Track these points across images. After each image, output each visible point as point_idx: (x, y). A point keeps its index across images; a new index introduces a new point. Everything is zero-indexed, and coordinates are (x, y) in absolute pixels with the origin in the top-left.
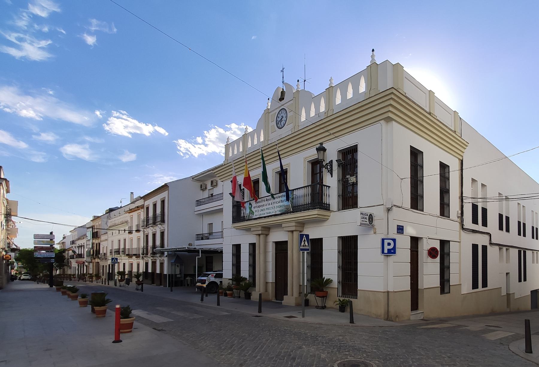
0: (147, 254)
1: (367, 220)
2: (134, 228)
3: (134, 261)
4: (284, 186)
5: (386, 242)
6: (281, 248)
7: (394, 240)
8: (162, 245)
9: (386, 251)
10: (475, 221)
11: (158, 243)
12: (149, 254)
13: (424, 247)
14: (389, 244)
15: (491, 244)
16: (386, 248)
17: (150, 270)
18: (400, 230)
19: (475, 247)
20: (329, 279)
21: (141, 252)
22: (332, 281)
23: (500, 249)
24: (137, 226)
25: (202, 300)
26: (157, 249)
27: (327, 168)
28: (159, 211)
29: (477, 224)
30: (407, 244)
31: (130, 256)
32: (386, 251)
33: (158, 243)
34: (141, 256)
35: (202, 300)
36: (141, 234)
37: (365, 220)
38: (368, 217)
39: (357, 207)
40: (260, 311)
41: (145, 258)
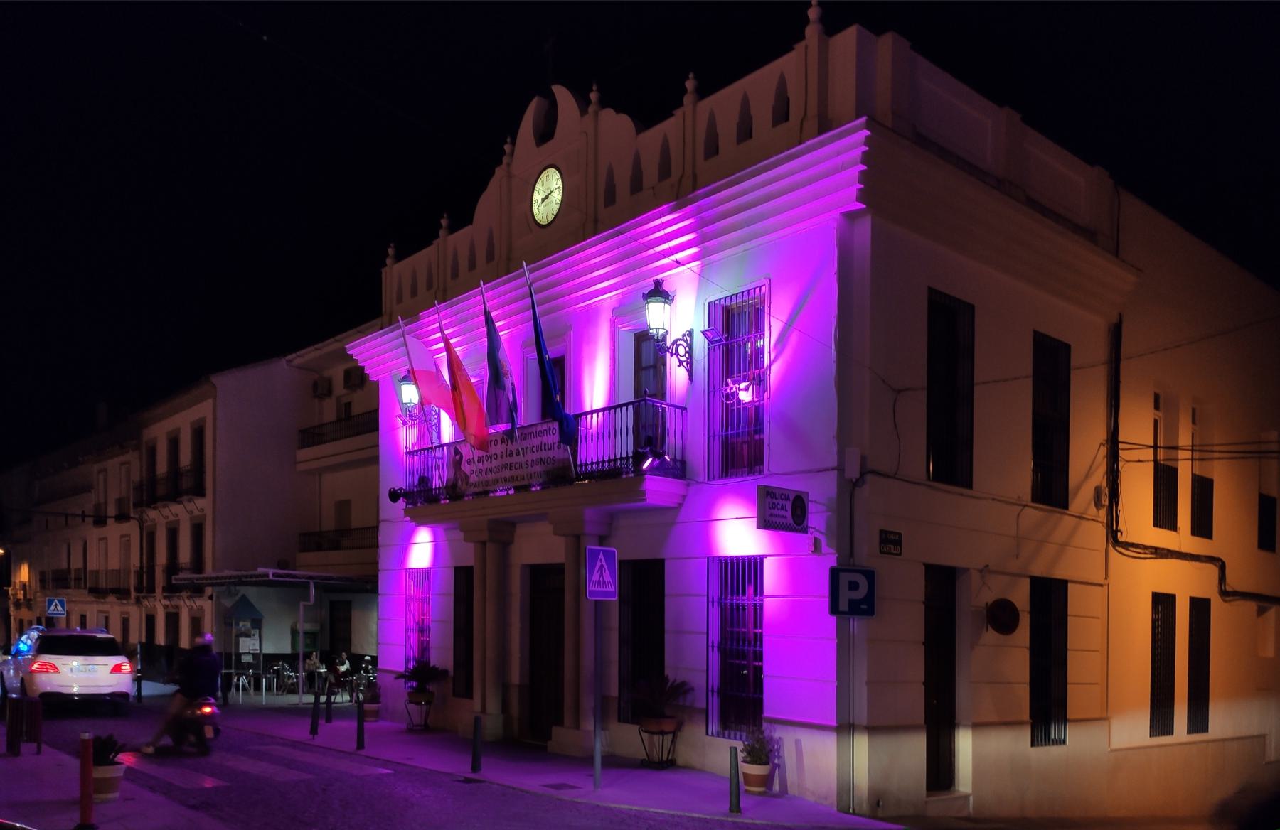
0: (151, 590)
1: (789, 514)
2: (112, 510)
3: (114, 608)
4: (648, 359)
5: (845, 579)
6: (547, 585)
7: (870, 575)
8: (198, 563)
9: (844, 606)
10: (1165, 516)
11: (185, 555)
12: (159, 590)
13: (975, 596)
14: (854, 586)
15: (1224, 593)
16: (845, 595)
17: (161, 639)
18: (890, 541)
19: (1163, 603)
20: (683, 684)
21: (133, 582)
22: (692, 689)
23: (1261, 612)
24: (120, 502)
25: (314, 731)
26: (181, 575)
27: (677, 354)
28: (185, 459)
29: (1173, 527)
30: (916, 587)
31: (98, 592)
32: (844, 606)
33: (185, 555)
34: (133, 594)
35: (314, 731)
36: (131, 528)
37: (781, 513)
38: (789, 505)
39: (761, 472)
40: (475, 769)
41: (145, 602)
